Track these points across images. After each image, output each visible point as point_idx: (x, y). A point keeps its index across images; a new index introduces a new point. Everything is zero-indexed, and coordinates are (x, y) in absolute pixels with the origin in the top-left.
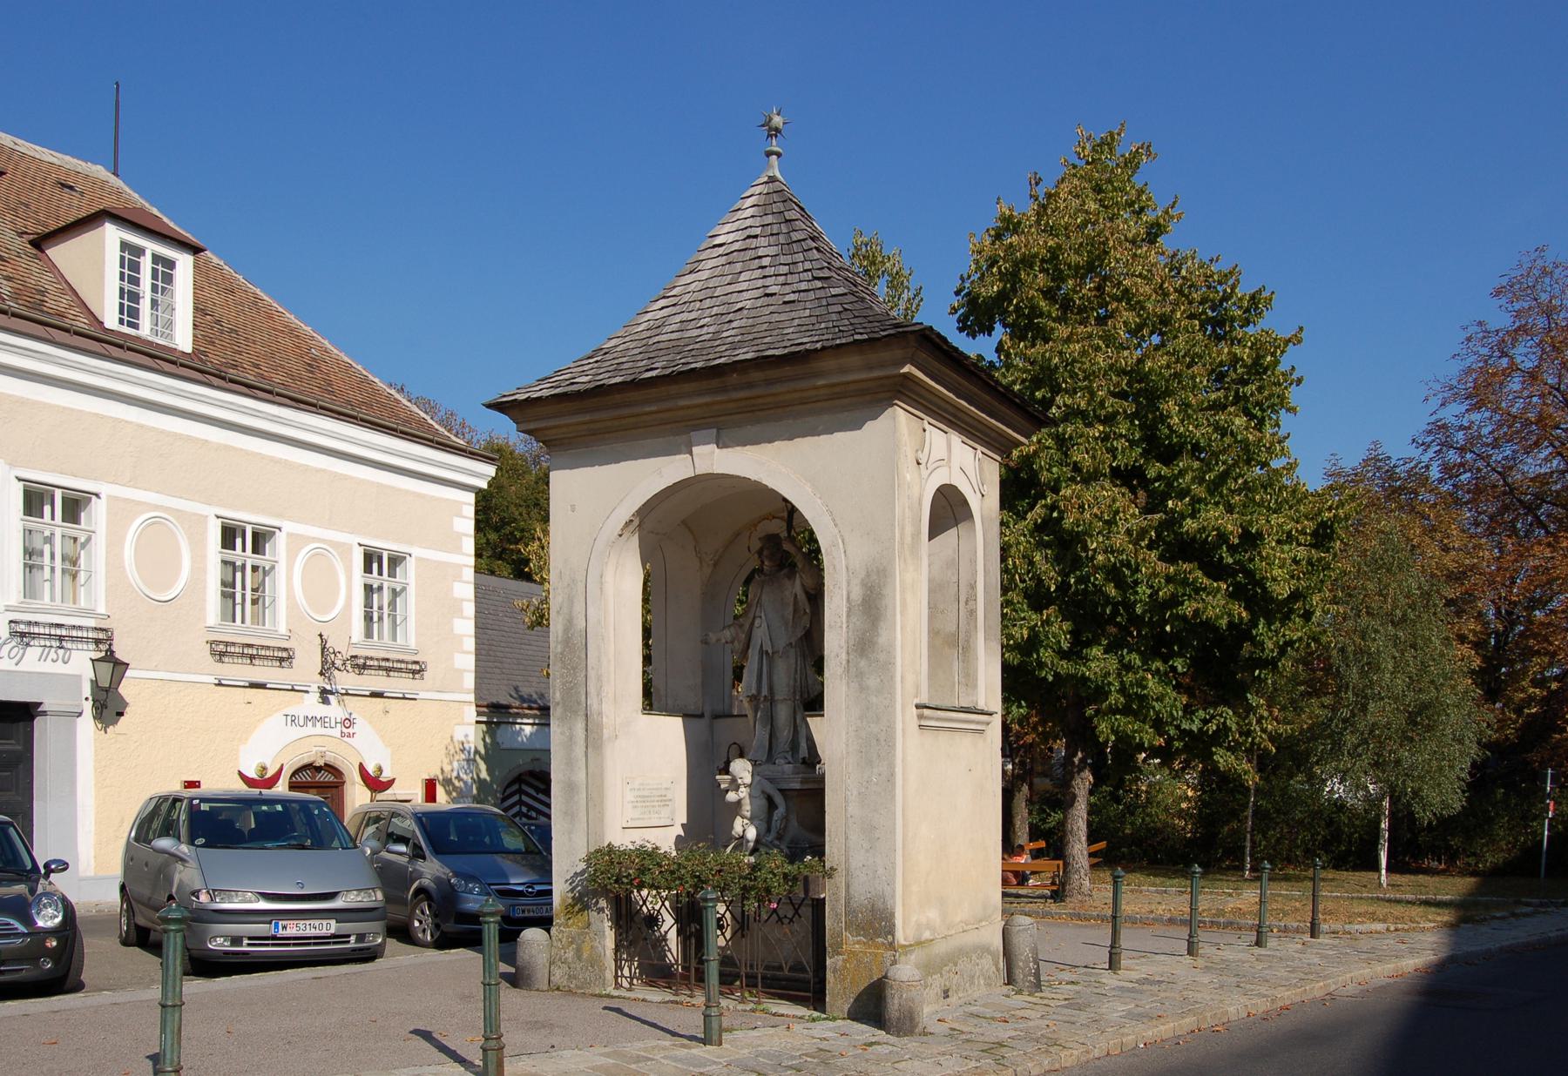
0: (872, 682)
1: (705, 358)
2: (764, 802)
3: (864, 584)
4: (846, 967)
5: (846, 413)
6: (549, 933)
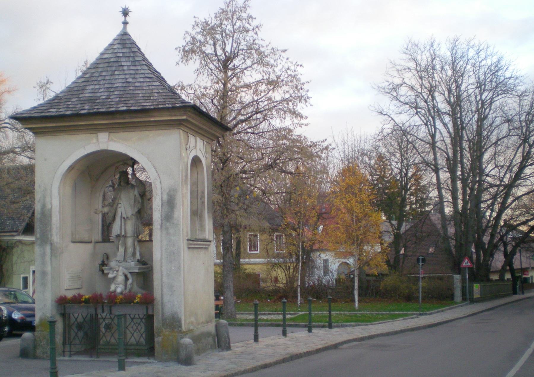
0: (171, 231)
1: (106, 107)
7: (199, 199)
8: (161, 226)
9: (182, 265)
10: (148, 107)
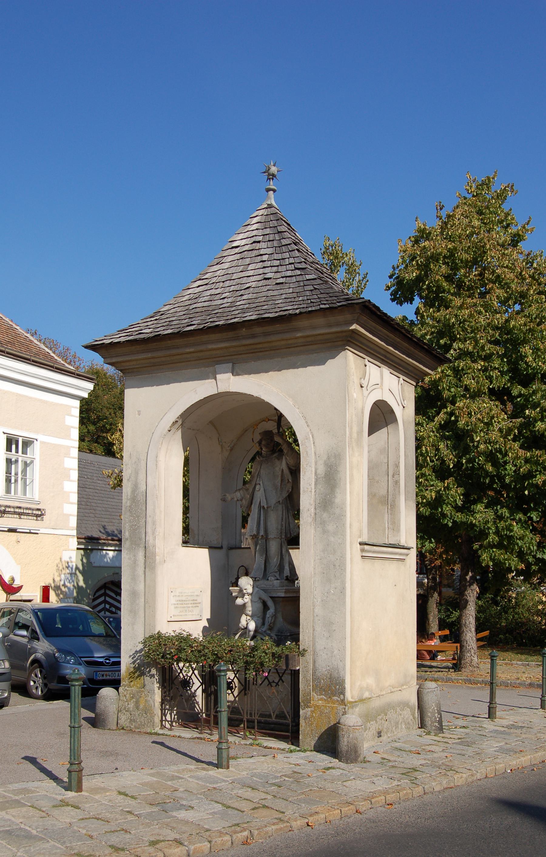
0: (331, 527)
2: (260, 605)
3: (326, 464)
4: (313, 716)
5: (315, 355)
6: (118, 691)
7: (390, 476)
8: (315, 519)
9: (348, 585)
10: (291, 312)
